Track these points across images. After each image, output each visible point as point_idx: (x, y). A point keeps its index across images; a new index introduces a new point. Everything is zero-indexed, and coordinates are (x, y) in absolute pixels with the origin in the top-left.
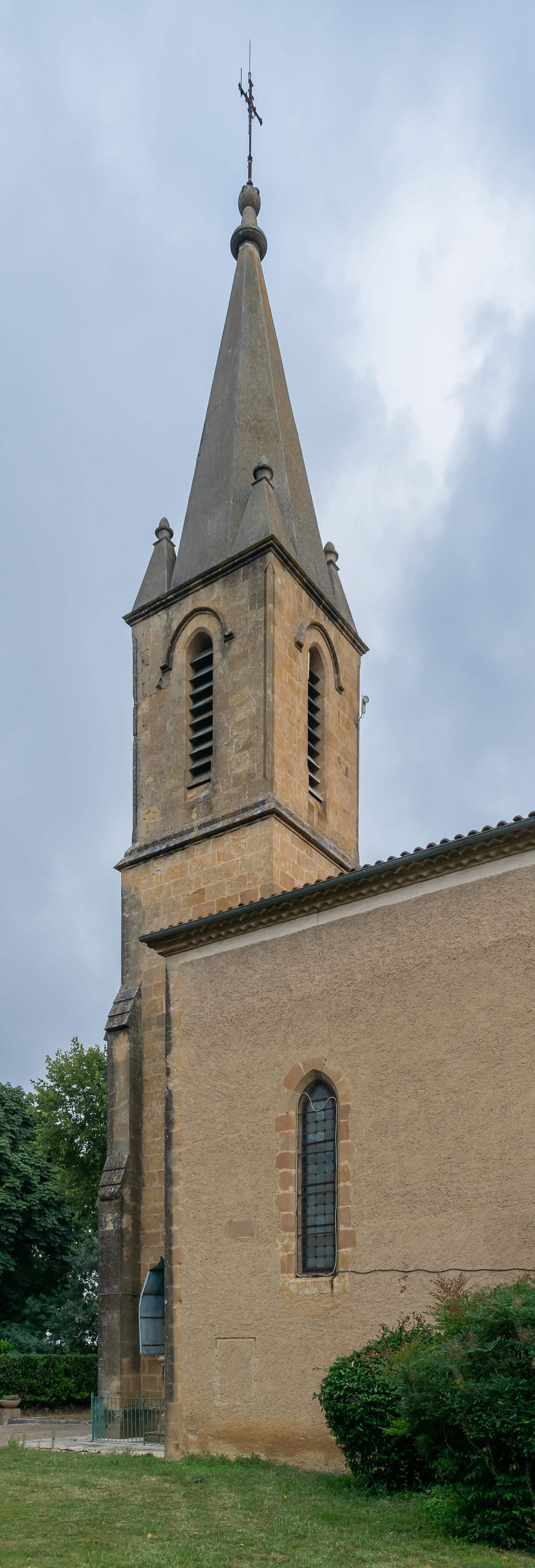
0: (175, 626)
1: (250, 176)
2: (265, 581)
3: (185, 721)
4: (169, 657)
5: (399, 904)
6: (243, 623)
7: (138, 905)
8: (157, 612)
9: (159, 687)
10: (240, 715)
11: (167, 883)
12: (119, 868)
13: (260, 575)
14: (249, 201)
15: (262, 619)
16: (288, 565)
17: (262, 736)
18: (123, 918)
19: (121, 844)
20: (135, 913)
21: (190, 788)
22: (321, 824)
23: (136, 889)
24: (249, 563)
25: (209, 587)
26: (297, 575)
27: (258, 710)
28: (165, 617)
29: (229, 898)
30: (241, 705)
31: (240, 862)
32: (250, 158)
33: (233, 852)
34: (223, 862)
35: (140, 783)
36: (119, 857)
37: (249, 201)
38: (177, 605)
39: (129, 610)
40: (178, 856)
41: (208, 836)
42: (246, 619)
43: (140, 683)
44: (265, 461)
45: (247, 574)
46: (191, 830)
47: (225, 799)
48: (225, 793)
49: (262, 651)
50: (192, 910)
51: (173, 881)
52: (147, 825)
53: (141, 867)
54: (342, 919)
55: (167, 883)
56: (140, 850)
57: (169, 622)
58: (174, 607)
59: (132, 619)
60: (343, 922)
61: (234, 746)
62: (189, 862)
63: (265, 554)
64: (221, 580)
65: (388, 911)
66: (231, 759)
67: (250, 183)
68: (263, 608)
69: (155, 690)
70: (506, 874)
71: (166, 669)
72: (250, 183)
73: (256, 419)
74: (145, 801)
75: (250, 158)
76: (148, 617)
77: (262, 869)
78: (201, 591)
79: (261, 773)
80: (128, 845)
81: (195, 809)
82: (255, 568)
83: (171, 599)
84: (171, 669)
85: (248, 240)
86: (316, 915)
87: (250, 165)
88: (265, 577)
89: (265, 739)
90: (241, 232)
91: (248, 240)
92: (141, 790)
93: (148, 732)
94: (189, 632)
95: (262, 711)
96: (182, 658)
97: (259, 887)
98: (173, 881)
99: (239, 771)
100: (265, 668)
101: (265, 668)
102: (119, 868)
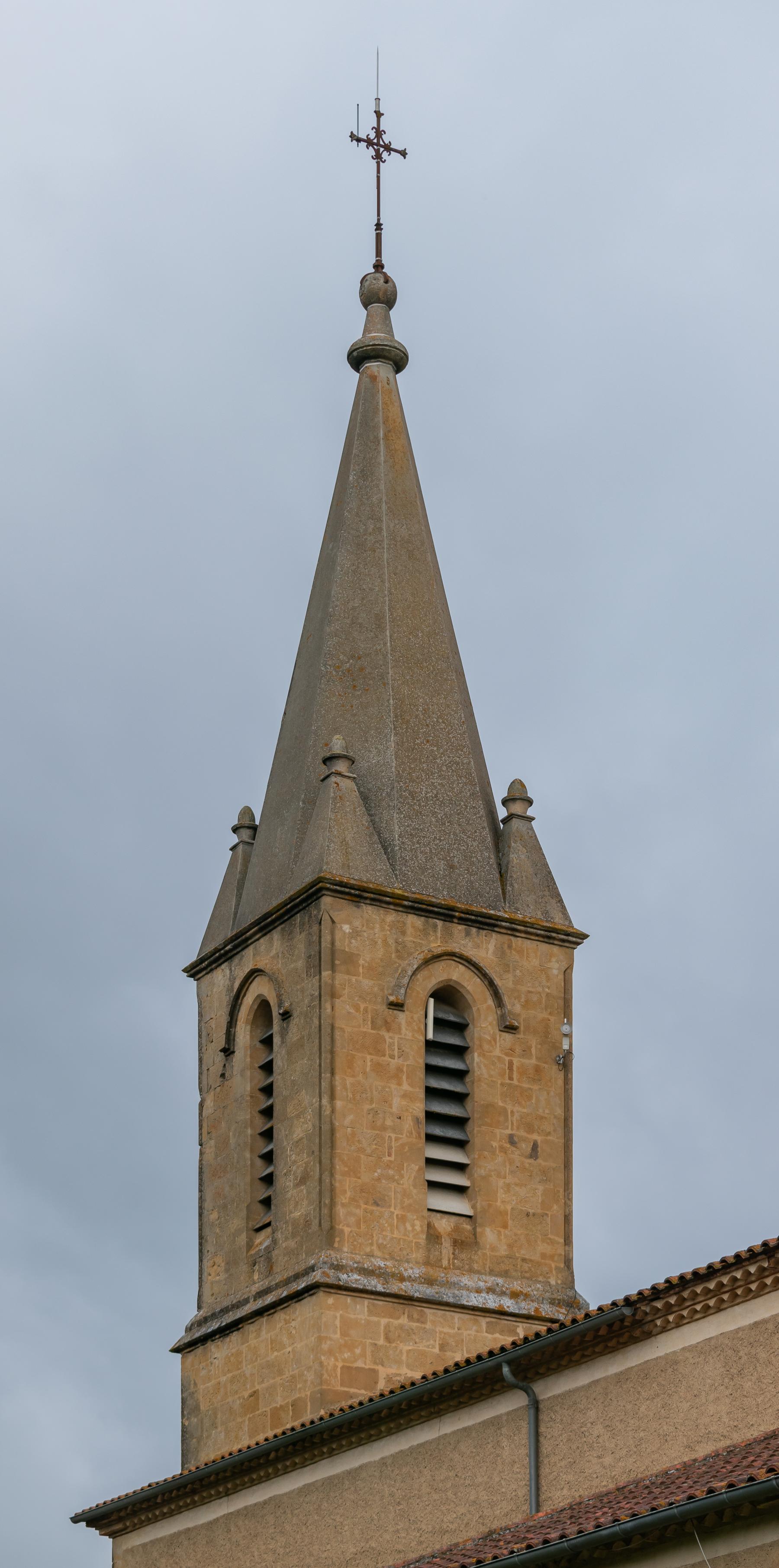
0: (237, 985)
1: (379, 253)
2: (320, 937)
3: (249, 1131)
4: (230, 1037)
5: (286, 1494)
6: (299, 998)
7: (197, 1408)
8: (220, 965)
9: (223, 1075)
10: (298, 1132)
11: (224, 1378)
12: (176, 1350)
13: (315, 928)
14: (379, 295)
15: (317, 993)
16: (366, 898)
17: (318, 1165)
18: (183, 1425)
19: (181, 1312)
20: (194, 1420)
21: (258, 1230)
22: (463, 1256)
23: (195, 1384)
24: (304, 908)
25: (268, 936)
26: (389, 903)
27: (314, 1126)
28: (228, 972)
29: (281, 1406)
30: (298, 1116)
31: (291, 1356)
32: (379, 226)
33: (285, 1339)
34: (276, 1353)
35: (205, 1220)
36: (178, 1335)
37: (379, 295)
38: (238, 956)
39: (192, 957)
40: (235, 1337)
41: (259, 1313)
42: (302, 991)
43: (205, 1068)
44: (337, 745)
45: (303, 924)
46: (246, 1301)
47: (284, 1255)
48: (284, 1245)
49: (317, 1041)
50: (247, 1422)
51: (230, 1375)
52: (212, 1283)
53: (200, 1350)
54: (246, 1508)
55: (224, 1378)
56: (205, 1320)
57: (232, 979)
58: (236, 960)
59: (195, 971)
60: (246, 1513)
61: (292, 1177)
62: (244, 1348)
63: (318, 898)
64: (279, 928)
65: (275, 1502)
66: (289, 1195)
67: (379, 266)
68: (317, 977)
69: (219, 1080)
70: (361, 1467)
71: (228, 1051)
72: (379, 266)
73: (353, 657)
74: (210, 1247)
75: (379, 226)
76: (212, 970)
77: (310, 1367)
78: (262, 940)
79: (317, 1221)
80: (191, 1313)
81: (257, 1267)
82: (310, 917)
83: (230, 950)
84: (233, 1052)
85: (376, 356)
86: (225, 1498)
87: (379, 238)
88: (320, 931)
89: (320, 1169)
90: (355, 354)
91: (376, 356)
92: (207, 1231)
93: (212, 1142)
94: (249, 1000)
95: (317, 1129)
96: (244, 1035)
97: (308, 1393)
98: (230, 1375)
99: (297, 1214)
100: (320, 1065)
101: (320, 1065)
102: (176, 1350)
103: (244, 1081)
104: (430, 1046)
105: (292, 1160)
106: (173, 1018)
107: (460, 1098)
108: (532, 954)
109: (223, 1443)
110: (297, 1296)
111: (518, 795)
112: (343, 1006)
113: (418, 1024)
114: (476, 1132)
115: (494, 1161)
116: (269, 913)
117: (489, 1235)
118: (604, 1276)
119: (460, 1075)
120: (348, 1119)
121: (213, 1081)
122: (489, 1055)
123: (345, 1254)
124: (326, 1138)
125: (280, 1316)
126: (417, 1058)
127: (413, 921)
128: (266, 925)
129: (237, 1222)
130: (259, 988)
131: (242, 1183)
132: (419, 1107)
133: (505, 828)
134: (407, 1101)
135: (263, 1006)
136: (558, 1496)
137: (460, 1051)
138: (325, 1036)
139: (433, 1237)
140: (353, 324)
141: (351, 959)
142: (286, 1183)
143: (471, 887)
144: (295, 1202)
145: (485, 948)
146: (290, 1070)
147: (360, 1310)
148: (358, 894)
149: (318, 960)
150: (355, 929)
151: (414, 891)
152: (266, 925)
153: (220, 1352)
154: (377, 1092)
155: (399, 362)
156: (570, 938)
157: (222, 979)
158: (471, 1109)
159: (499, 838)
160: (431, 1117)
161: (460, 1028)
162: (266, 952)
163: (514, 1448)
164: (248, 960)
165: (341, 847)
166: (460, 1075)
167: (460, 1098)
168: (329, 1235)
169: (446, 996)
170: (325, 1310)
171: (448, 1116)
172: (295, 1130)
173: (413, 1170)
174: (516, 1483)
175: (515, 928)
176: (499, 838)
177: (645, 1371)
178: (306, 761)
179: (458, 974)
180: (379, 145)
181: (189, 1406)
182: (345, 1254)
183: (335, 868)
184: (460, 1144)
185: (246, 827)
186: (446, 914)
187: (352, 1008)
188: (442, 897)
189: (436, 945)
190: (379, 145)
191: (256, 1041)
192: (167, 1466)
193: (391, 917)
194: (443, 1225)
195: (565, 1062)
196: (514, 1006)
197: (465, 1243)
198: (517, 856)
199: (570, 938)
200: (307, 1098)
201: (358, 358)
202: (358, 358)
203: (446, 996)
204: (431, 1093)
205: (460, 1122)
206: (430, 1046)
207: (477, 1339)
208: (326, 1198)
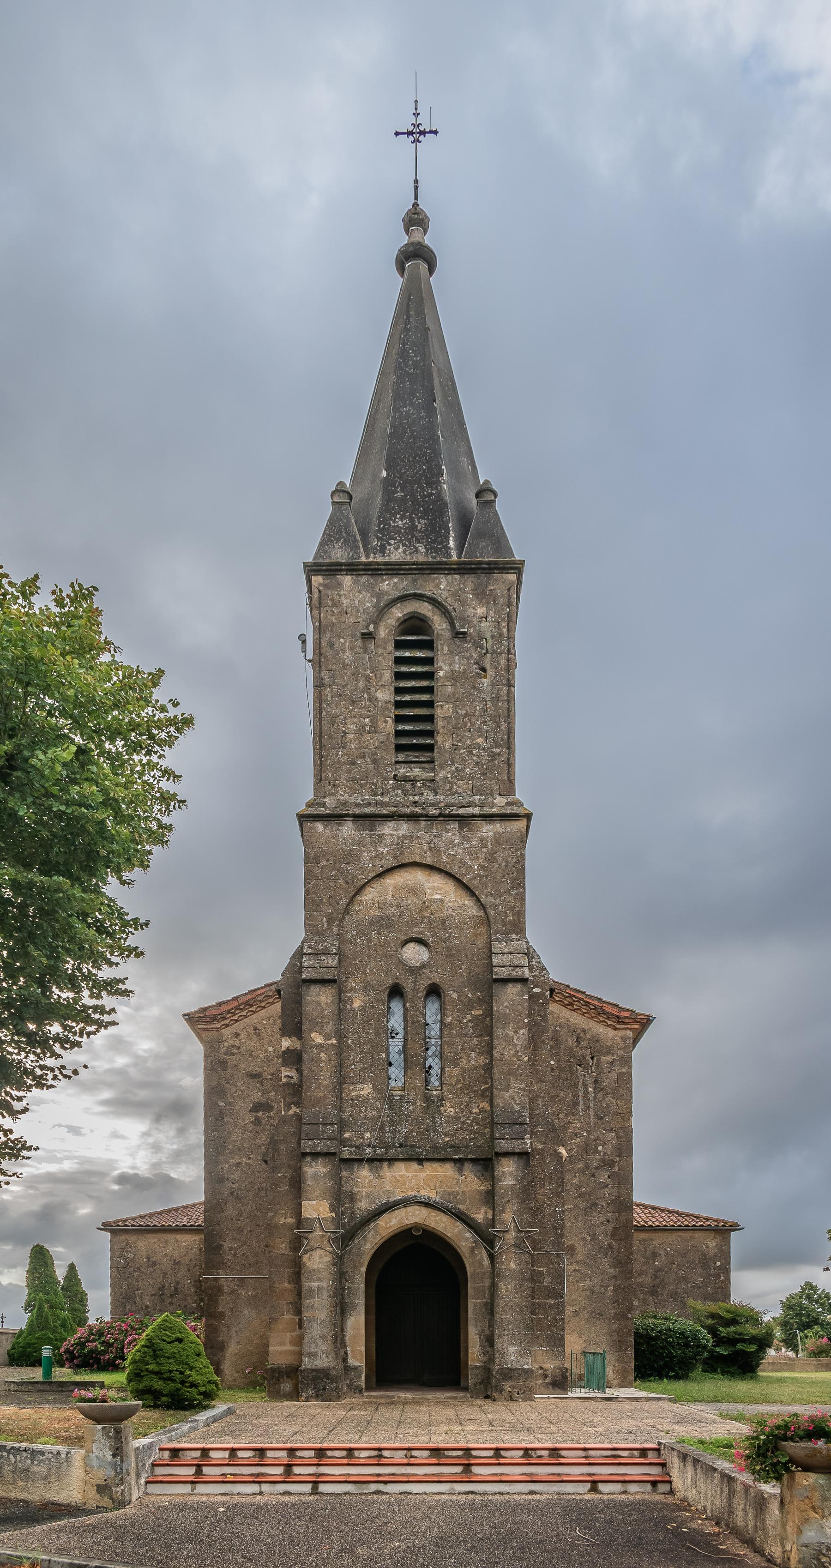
14: (415, 219)
67: (415, 205)
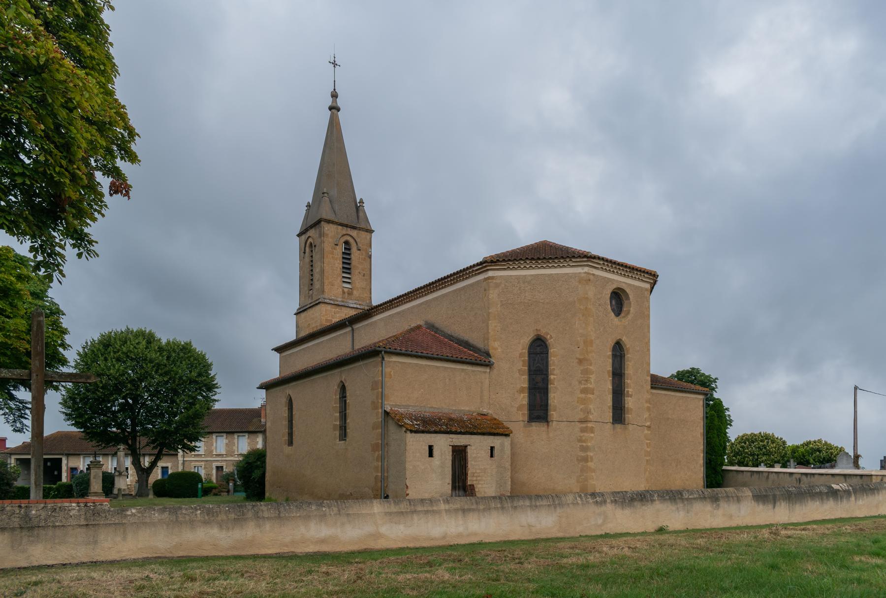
6: (317, 242)
14: (334, 95)
19: (296, 306)
36: (295, 311)
37: (334, 95)
44: (325, 190)
59: (299, 235)
80: (298, 307)
85: (334, 108)
91: (334, 108)
103: (307, 259)
104: (343, 253)
105: (316, 276)
106: (295, 243)
107: (349, 264)
108: (363, 234)
109: (303, 334)
110: (317, 304)
111: (361, 202)
112: (326, 244)
113: (341, 248)
114: (353, 271)
115: (356, 277)
116: (312, 225)
117: (355, 292)
118: (377, 299)
119: (349, 259)
120: (327, 268)
121: (302, 259)
122: (355, 255)
123: (326, 296)
124: (322, 271)
125: (314, 308)
126: (340, 256)
127: (340, 227)
128: (311, 227)
129: (306, 288)
130: (310, 240)
131: (307, 280)
132: (341, 266)
133: (358, 208)
134: (339, 264)
135: (311, 244)
136: (356, 347)
137: (349, 254)
138: (322, 251)
139: (344, 292)
140: (329, 102)
141: (327, 235)
142: (315, 280)
143: (352, 221)
144: (317, 285)
145: (354, 233)
146: (316, 257)
147: (329, 307)
148: (329, 222)
149: (321, 235)
150: (327, 228)
151: (340, 221)
152: (311, 227)
153: (303, 315)
154: (333, 262)
155: (338, 110)
156: (371, 231)
157: (304, 237)
158: (352, 266)
159: (357, 208)
160: (343, 268)
161: (349, 249)
162: (311, 233)
163: (349, 338)
164: (309, 234)
165: (326, 212)
166: (349, 259)
167: (349, 264)
168: (323, 292)
169: (347, 243)
170: (322, 307)
171: (347, 268)
172: (317, 270)
173: (340, 278)
174: (349, 345)
175: (360, 229)
176: (357, 208)
177: (371, 324)
178: (320, 193)
179: (349, 238)
180: (335, 64)
181: (297, 326)
182: (326, 296)
183: (324, 216)
184: (349, 273)
185: (308, 206)
186: (347, 226)
187: (328, 245)
188: (346, 222)
189: (344, 232)
190: (335, 64)
191: (310, 250)
192: (292, 337)
193: (335, 226)
194: (346, 290)
195: (370, 257)
196: (360, 245)
197: (350, 294)
198: (361, 214)
199: (371, 231)
200: (319, 263)
201: (331, 108)
202: (331, 108)
203: (347, 243)
204: (343, 263)
205: (349, 269)
206: (343, 253)
207: (353, 313)
208: (322, 284)
